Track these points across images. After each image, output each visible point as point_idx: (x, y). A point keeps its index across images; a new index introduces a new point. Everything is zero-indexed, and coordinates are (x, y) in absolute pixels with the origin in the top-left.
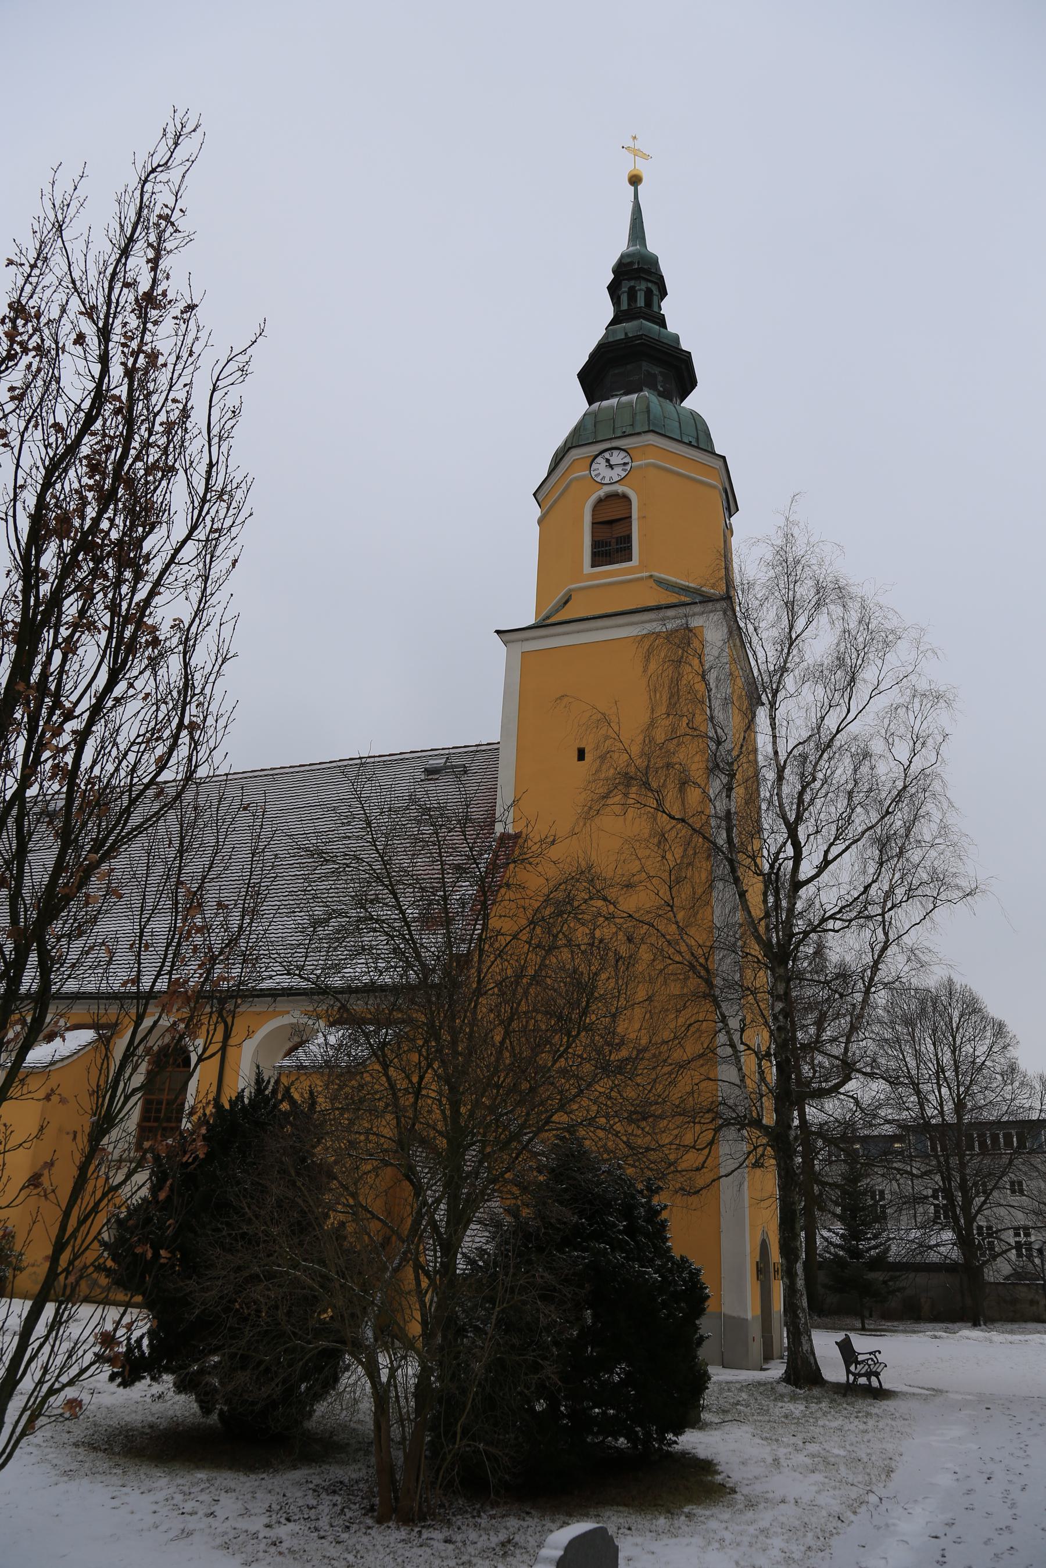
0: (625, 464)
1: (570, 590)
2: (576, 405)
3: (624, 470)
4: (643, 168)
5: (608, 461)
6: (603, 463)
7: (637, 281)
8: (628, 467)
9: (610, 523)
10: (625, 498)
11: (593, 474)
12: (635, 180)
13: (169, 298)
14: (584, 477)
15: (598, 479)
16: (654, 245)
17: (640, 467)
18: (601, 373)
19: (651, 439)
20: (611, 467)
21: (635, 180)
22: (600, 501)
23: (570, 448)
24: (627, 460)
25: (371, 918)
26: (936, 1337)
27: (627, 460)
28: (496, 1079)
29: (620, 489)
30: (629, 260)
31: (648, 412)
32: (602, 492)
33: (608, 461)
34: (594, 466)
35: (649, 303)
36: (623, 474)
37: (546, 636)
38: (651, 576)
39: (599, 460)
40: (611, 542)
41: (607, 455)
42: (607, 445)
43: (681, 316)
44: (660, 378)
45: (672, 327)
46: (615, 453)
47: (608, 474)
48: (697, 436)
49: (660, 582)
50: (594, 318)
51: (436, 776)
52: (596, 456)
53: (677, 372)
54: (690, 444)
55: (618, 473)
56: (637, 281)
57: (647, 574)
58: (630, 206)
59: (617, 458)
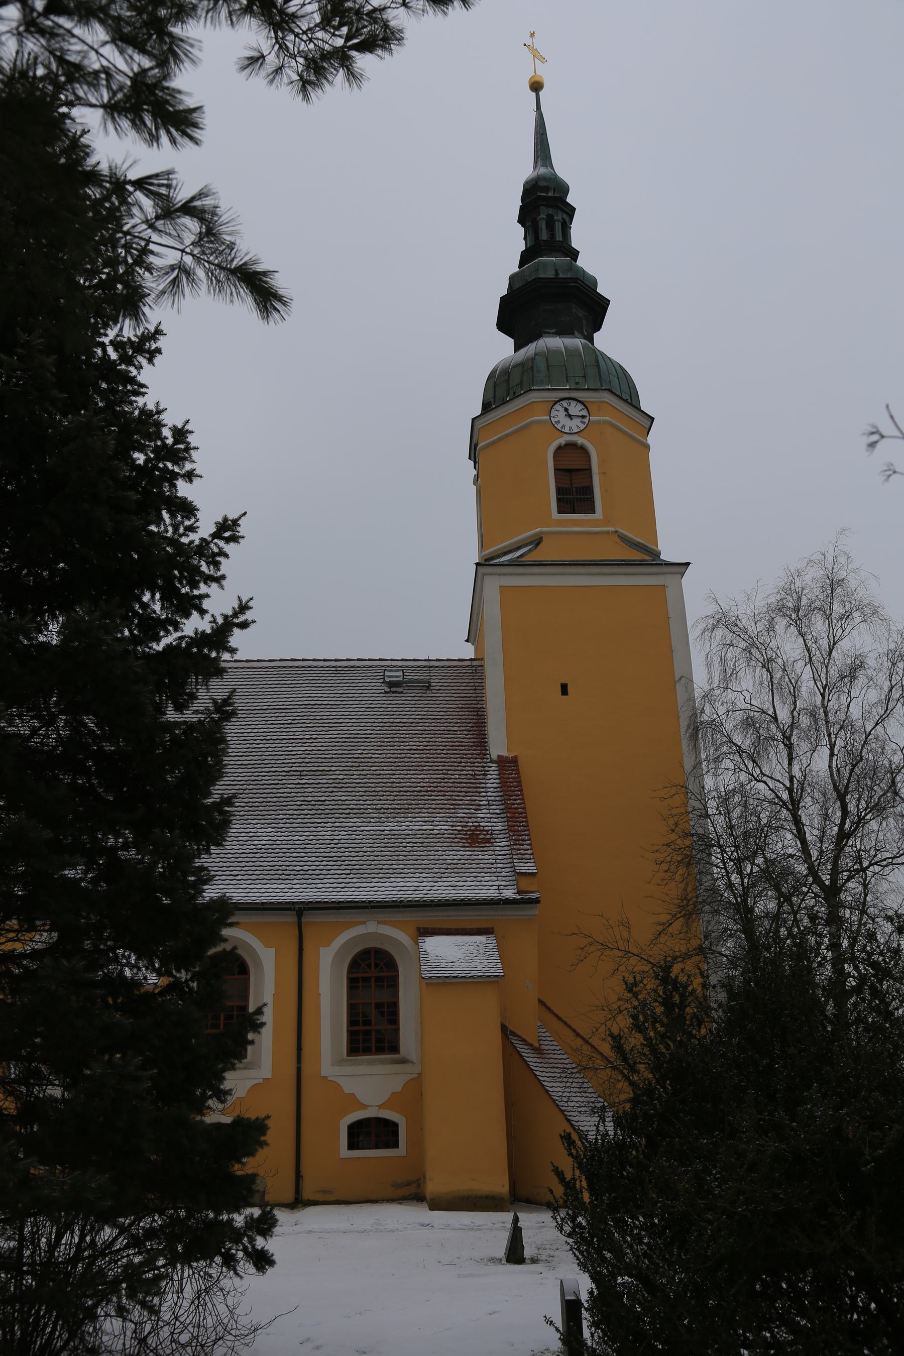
0: (583, 417)
1: (541, 533)
2: (502, 349)
3: (584, 423)
4: (545, 74)
5: (566, 410)
6: (562, 413)
7: (545, 207)
8: (586, 420)
9: (569, 471)
10: (583, 449)
12: (536, 87)
15: (559, 427)
16: (563, 167)
18: (518, 313)
19: (607, 397)
20: (570, 416)
21: (536, 87)
22: (560, 448)
24: (585, 412)
25: (795, 913)
26: (324, 1192)
27: (585, 412)
29: (580, 440)
30: (545, 184)
31: (598, 366)
32: (563, 440)
33: (566, 410)
34: (553, 413)
36: (582, 426)
37: (523, 574)
38: (616, 532)
39: (557, 407)
41: (565, 403)
42: (566, 395)
43: (595, 246)
44: (584, 322)
46: (573, 403)
49: (624, 539)
51: (400, 690)
52: (556, 402)
53: (585, 306)
54: (626, 401)
55: (576, 425)
56: (545, 207)
57: (612, 529)
58: (534, 115)
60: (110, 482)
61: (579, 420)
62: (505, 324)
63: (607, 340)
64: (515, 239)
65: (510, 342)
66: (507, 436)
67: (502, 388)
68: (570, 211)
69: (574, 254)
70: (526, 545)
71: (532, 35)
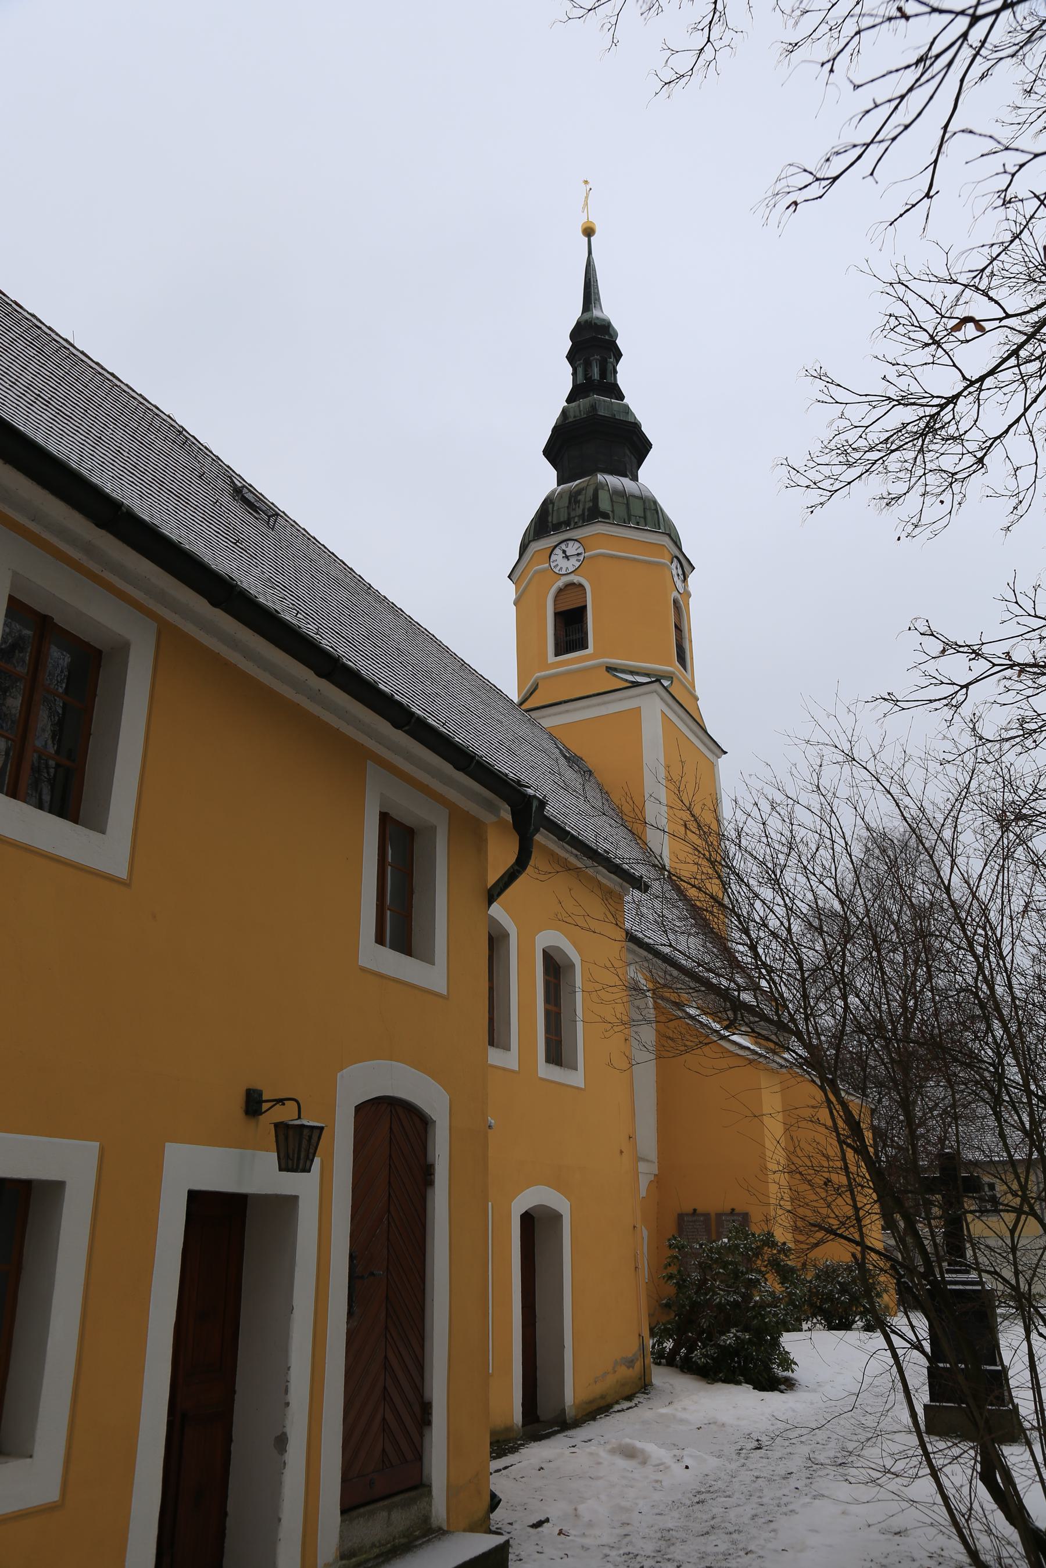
0: (578, 554)
2: (545, 480)
3: (578, 560)
5: (564, 552)
7: (594, 347)
10: (581, 585)
11: (553, 565)
13: (863, 1453)
14: (544, 570)
16: (610, 309)
17: (591, 557)
18: (566, 446)
20: (567, 557)
22: (560, 591)
23: (530, 542)
24: (581, 550)
28: (986, 1074)
29: (575, 579)
32: (560, 583)
33: (564, 552)
34: (553, 557)
35: (603, 373)
36: (578, 564)
39: (558, 551)
40: (571, 628)
41: (563, 546)
43: (641, 386)
45: (631, 400)
46: (571, 543)
47: (564, 563)
48: (648, 514)
50: (549, 389)
52: (556, 546)
53: (629, 444)
56: (594, 347)
59: (572, 549)
60: (760, 951)
61: (576, 558)
62: (552, 452)
63: (653, 477)
64: (562, 379)
65: (552, 473)
66: (634, 560)
67: (545, 523)
68: (618, 355)
69: (621, 396)
70: (648, 675)
71: (586, 182)
